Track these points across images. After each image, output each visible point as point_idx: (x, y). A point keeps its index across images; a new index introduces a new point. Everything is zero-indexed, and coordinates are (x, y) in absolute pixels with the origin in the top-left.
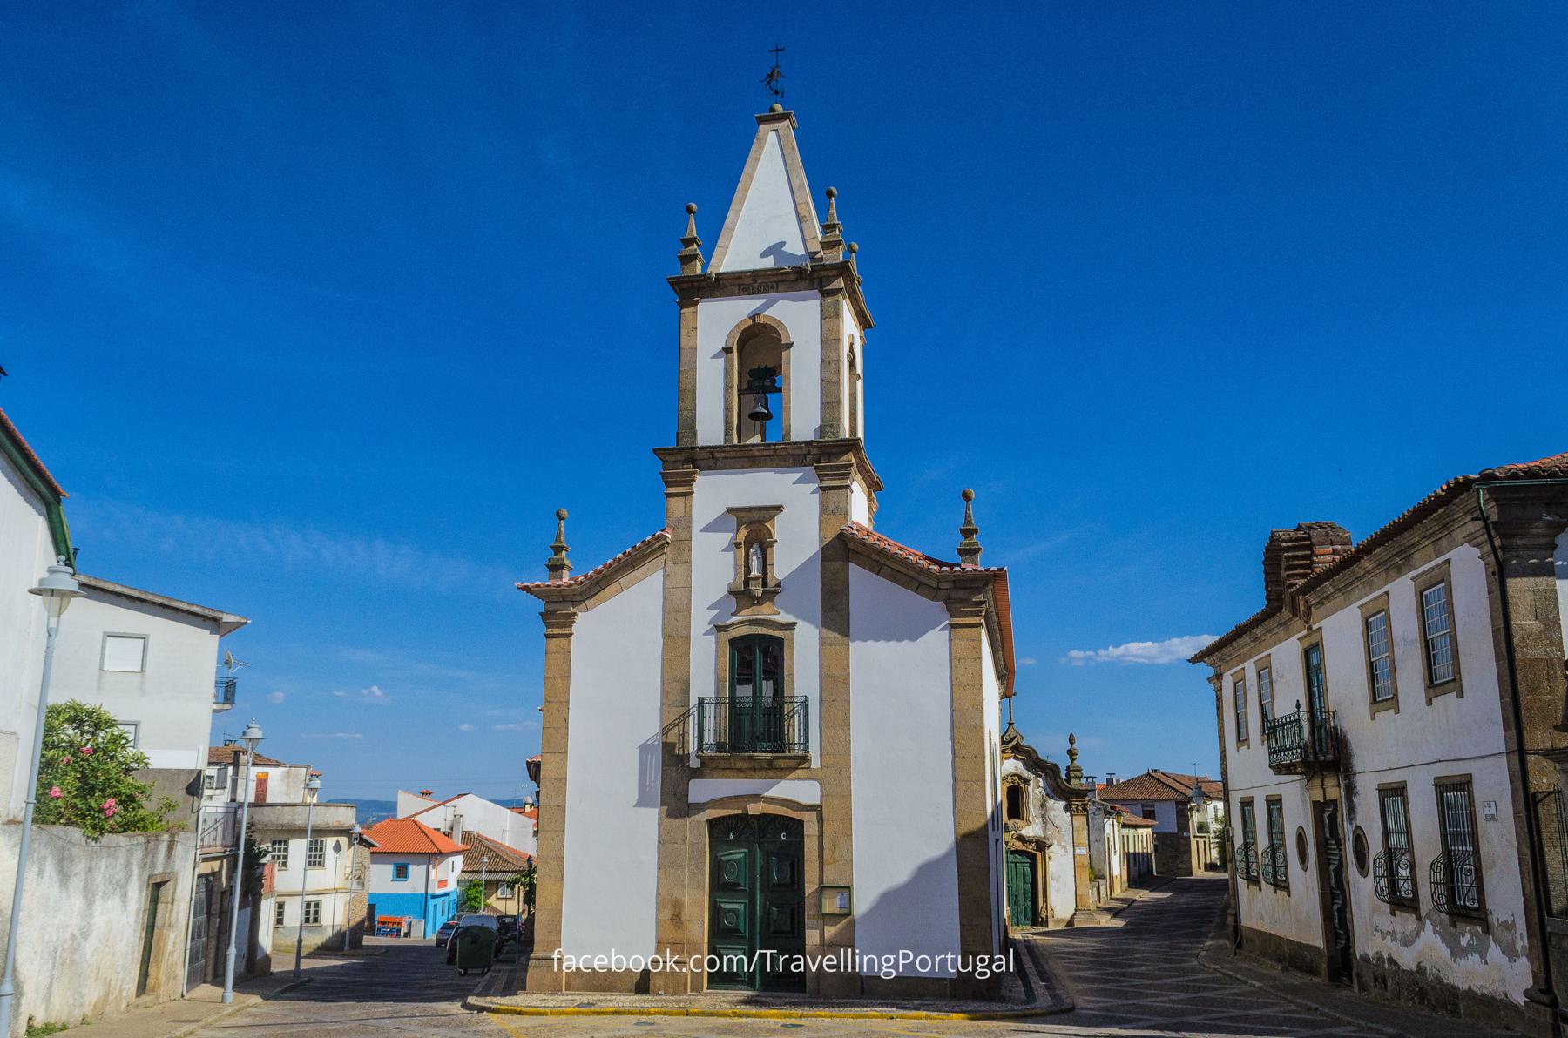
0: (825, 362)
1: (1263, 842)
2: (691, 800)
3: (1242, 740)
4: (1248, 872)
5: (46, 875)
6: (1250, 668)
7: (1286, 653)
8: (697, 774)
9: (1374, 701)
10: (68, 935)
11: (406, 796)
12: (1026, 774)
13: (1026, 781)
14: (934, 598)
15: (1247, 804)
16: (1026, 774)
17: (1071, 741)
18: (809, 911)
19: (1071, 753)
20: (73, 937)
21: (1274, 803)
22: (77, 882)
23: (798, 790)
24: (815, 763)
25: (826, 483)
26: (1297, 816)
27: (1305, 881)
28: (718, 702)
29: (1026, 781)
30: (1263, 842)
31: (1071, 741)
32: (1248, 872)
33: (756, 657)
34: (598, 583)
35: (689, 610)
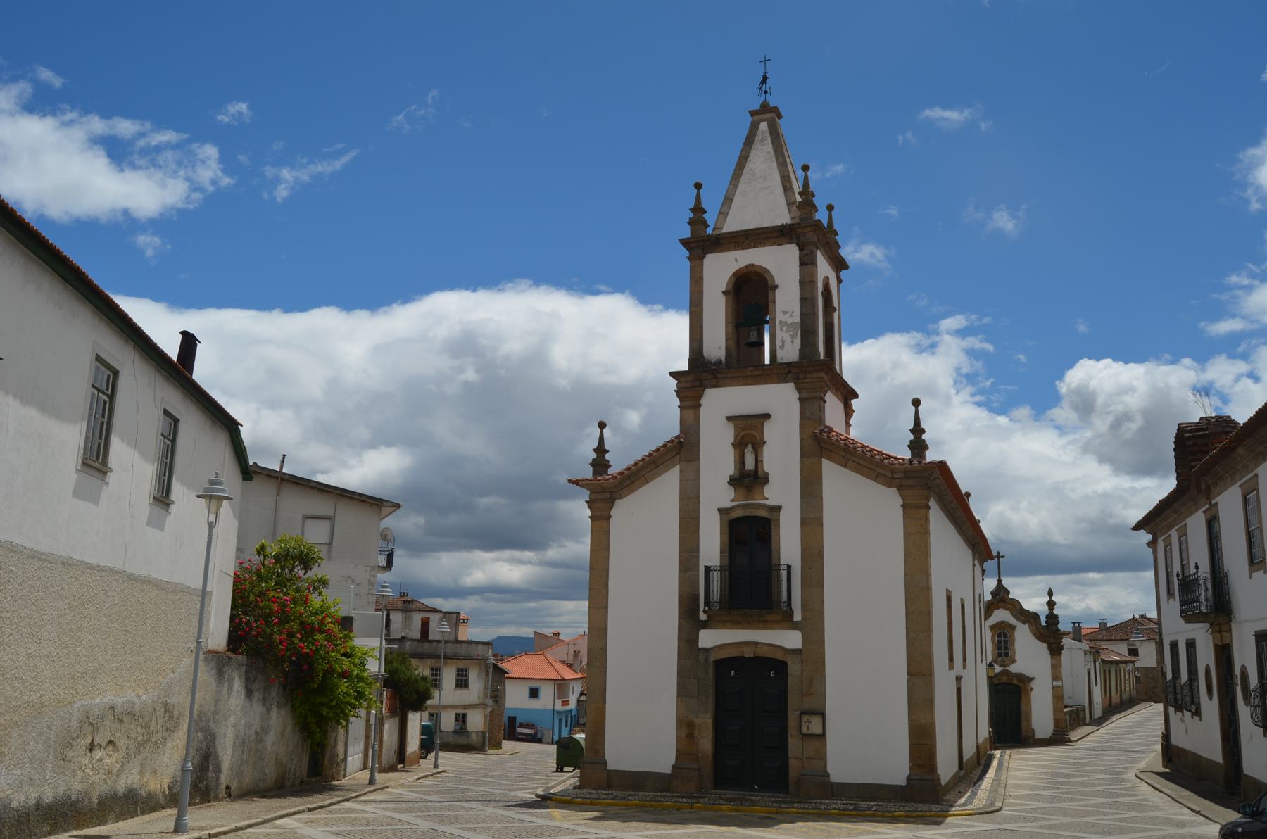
0: (803, 300)
1: (1184, 677)
2: (701, 645)
3: (1170, 594)
4: (1176, 700)
5: (235, 693)
6: (1174, 534)
7: (1196, 523)
8: (705, 625)
9: (1252, 562)
10: (252, 731)
11: (1205, 753)
12: (1013, 621)
13: (1014, 628)
14: (890, 486)
15: (1174, 646)
16: (1013, 621)
17: (1050, 593)
18: (792, 730)
19: (1051, 604)
20: (257, 733)
21: (1191, 645)
22: (257, 695)
23: (791, 639)
24: (797, 617)
25: (805, 395)
26: (1206, 657)
27: (1211, 708)
28: (722, 568)
29: (1014, 628)
30: (1184, 677)
31: (1050, 593)
32: (1176, 700)
33: (750, 534)
34: (628, 477)
35: (698, 497)
